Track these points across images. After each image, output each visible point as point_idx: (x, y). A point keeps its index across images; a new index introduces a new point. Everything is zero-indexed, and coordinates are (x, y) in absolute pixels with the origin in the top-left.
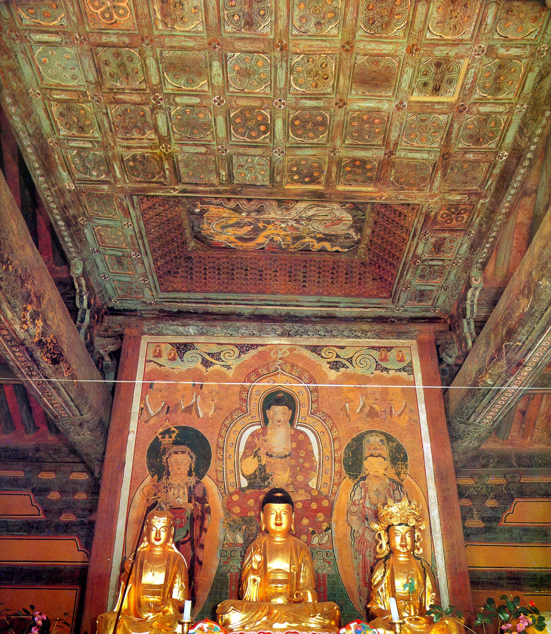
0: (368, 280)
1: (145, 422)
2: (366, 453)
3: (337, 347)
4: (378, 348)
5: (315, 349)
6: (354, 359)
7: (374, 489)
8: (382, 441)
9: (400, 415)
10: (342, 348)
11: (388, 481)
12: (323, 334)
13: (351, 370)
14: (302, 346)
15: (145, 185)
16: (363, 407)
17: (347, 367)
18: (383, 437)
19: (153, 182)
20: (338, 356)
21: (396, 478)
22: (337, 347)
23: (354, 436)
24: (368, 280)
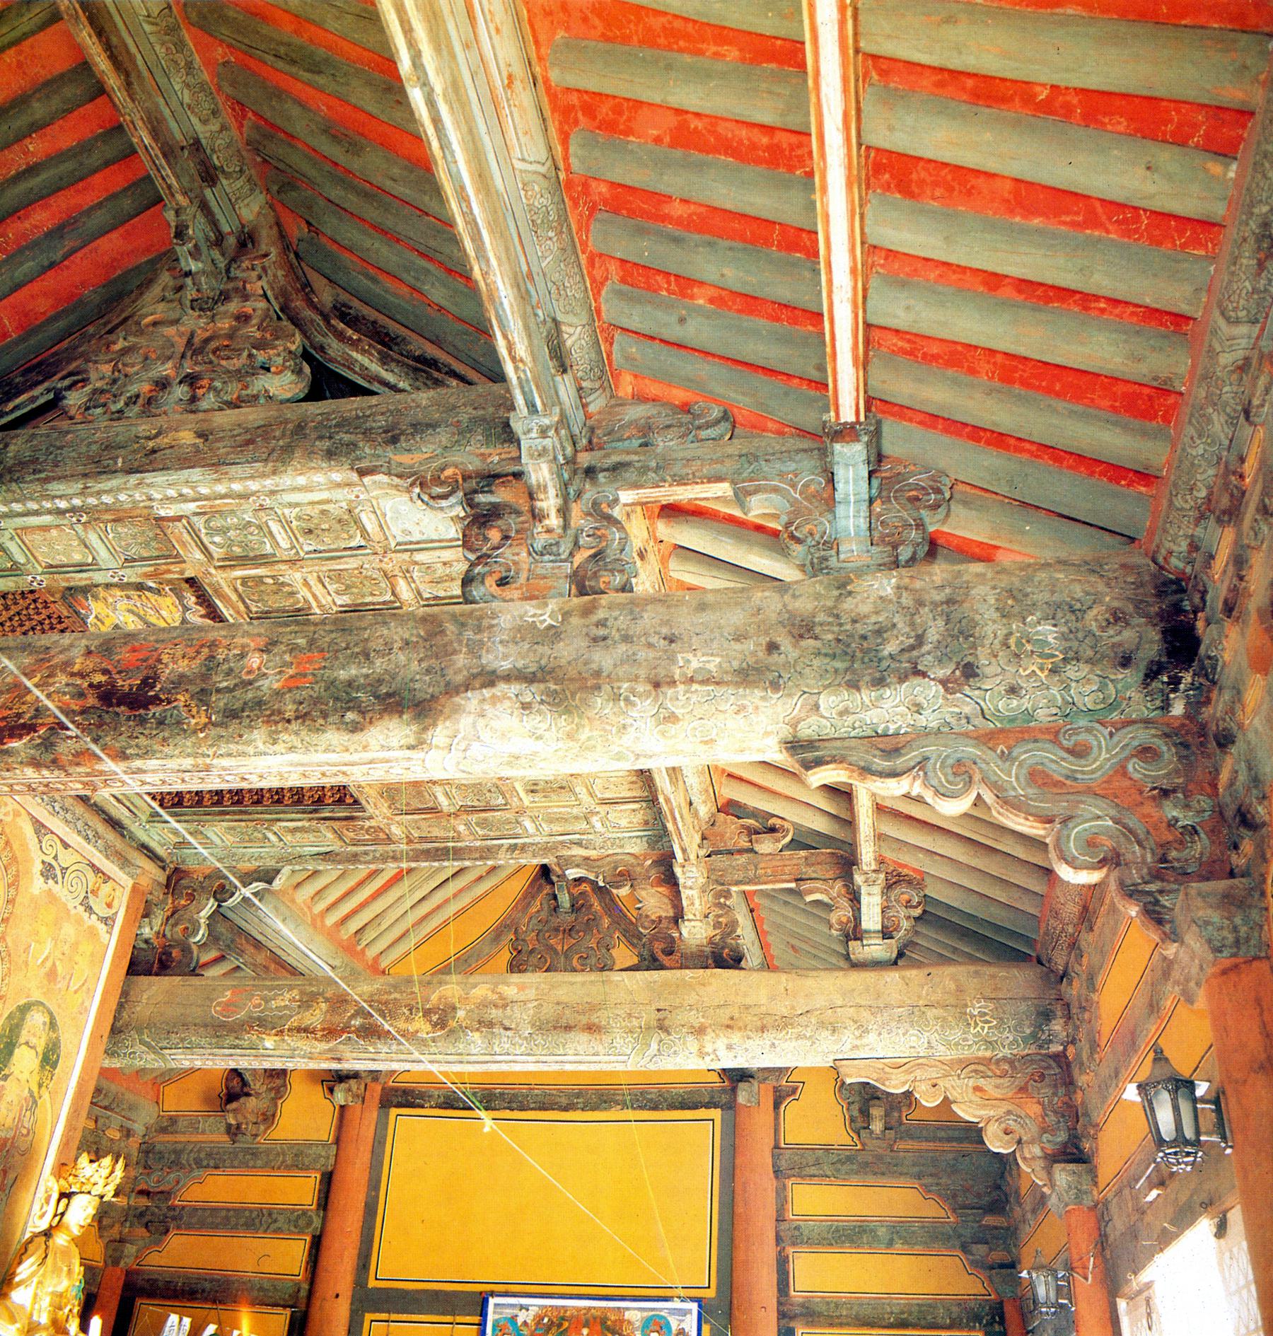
0: (214, 126)
1: (563, 369)
2: (22, 1040)
3: (62, 840)
4: (96, 870)
5: (39, 827)
6: (69, 871)
7: (9, 1099)
8: (45, 1024)
9: (76, 992)
10: (66, 846)
11: (26, 1091)
12: (57, 809)
13: (57, 889)
14: (29, 814)
15: (234, 597)
16: (47, 959)
17: (57, 882)
18: (47, 1020)
19: (244, 602)
20: (55, 858)
21: (35, 1089)
22: (62, 840)
23: (22, 1002)
24: (214, 126)
